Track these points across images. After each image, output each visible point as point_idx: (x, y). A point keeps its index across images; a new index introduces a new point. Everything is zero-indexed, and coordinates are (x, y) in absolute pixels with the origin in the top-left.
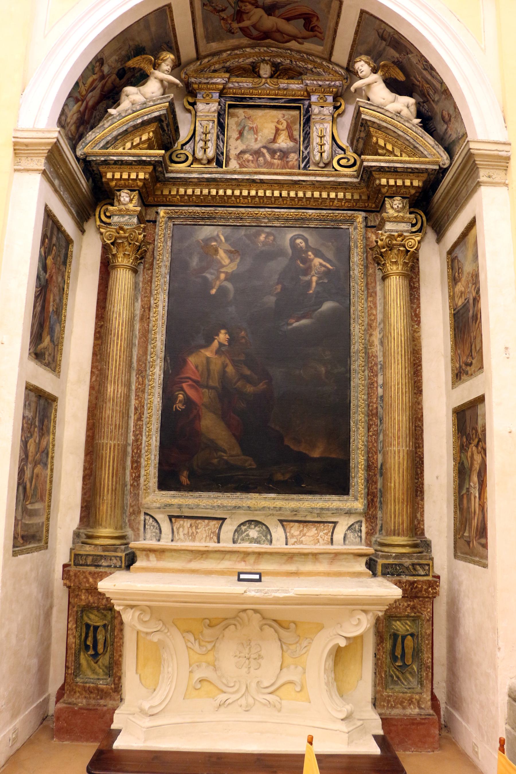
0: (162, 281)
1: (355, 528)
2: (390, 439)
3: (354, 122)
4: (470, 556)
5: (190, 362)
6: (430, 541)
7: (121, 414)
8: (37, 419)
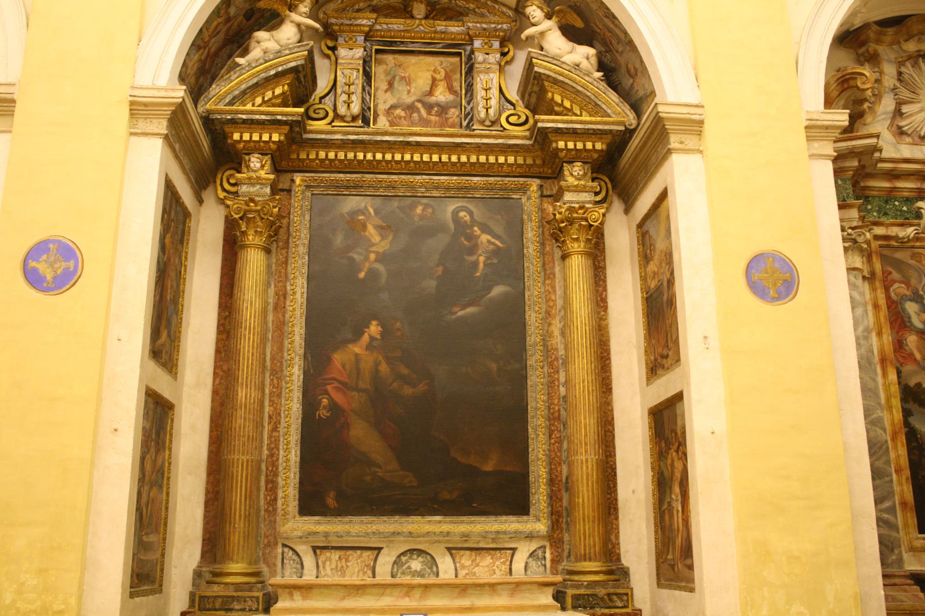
0: (300, 262)
1: (538, 555)
2: (575, 446)
3: (525, 74)
4: (676, 582)
5: (335, 360)
6: (628, 568)
7: (255, 423)
8: (154, 431)
